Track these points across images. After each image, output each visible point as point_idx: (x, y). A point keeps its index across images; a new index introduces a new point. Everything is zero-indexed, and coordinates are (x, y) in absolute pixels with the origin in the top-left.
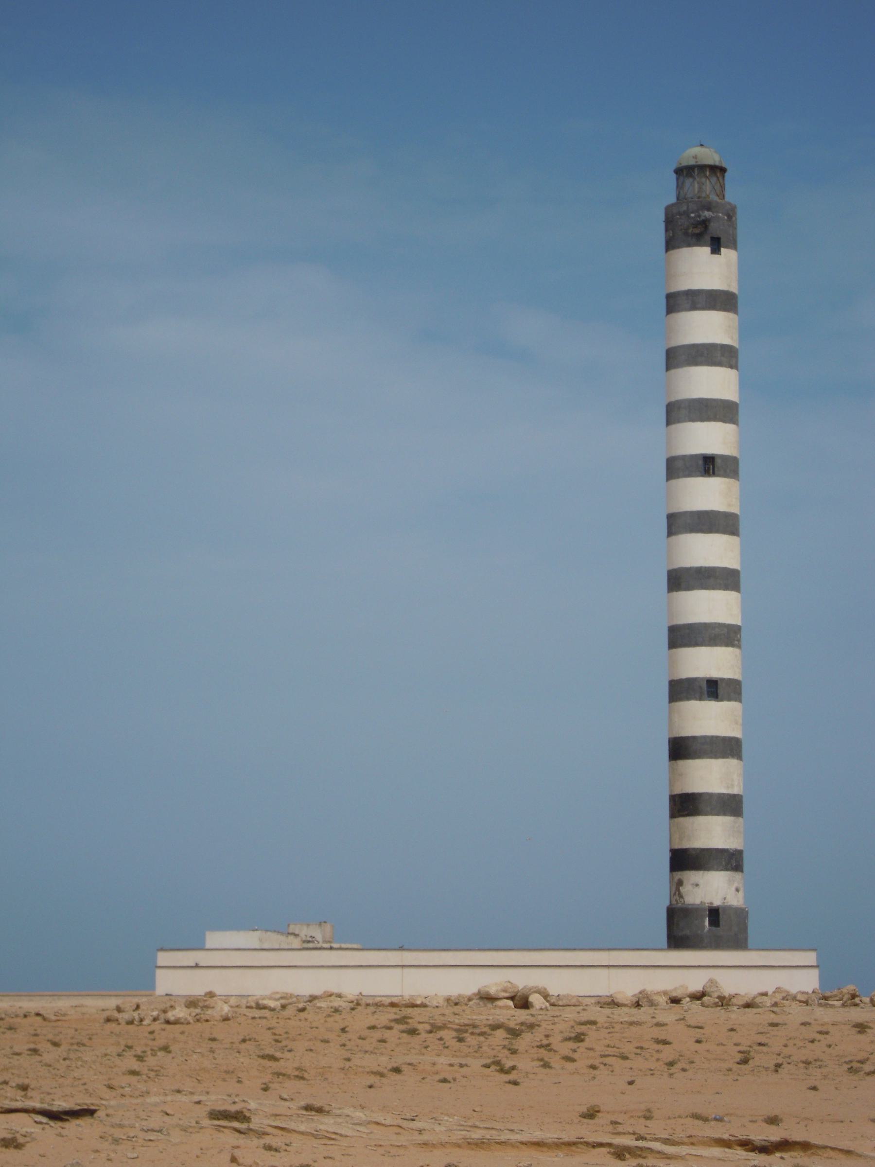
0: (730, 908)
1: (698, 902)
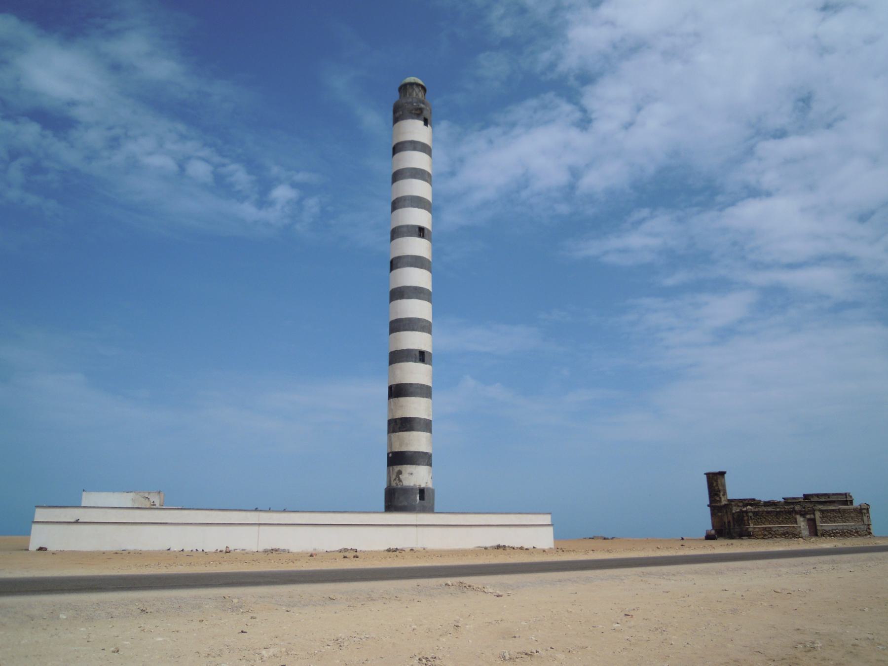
1: (412, 484)
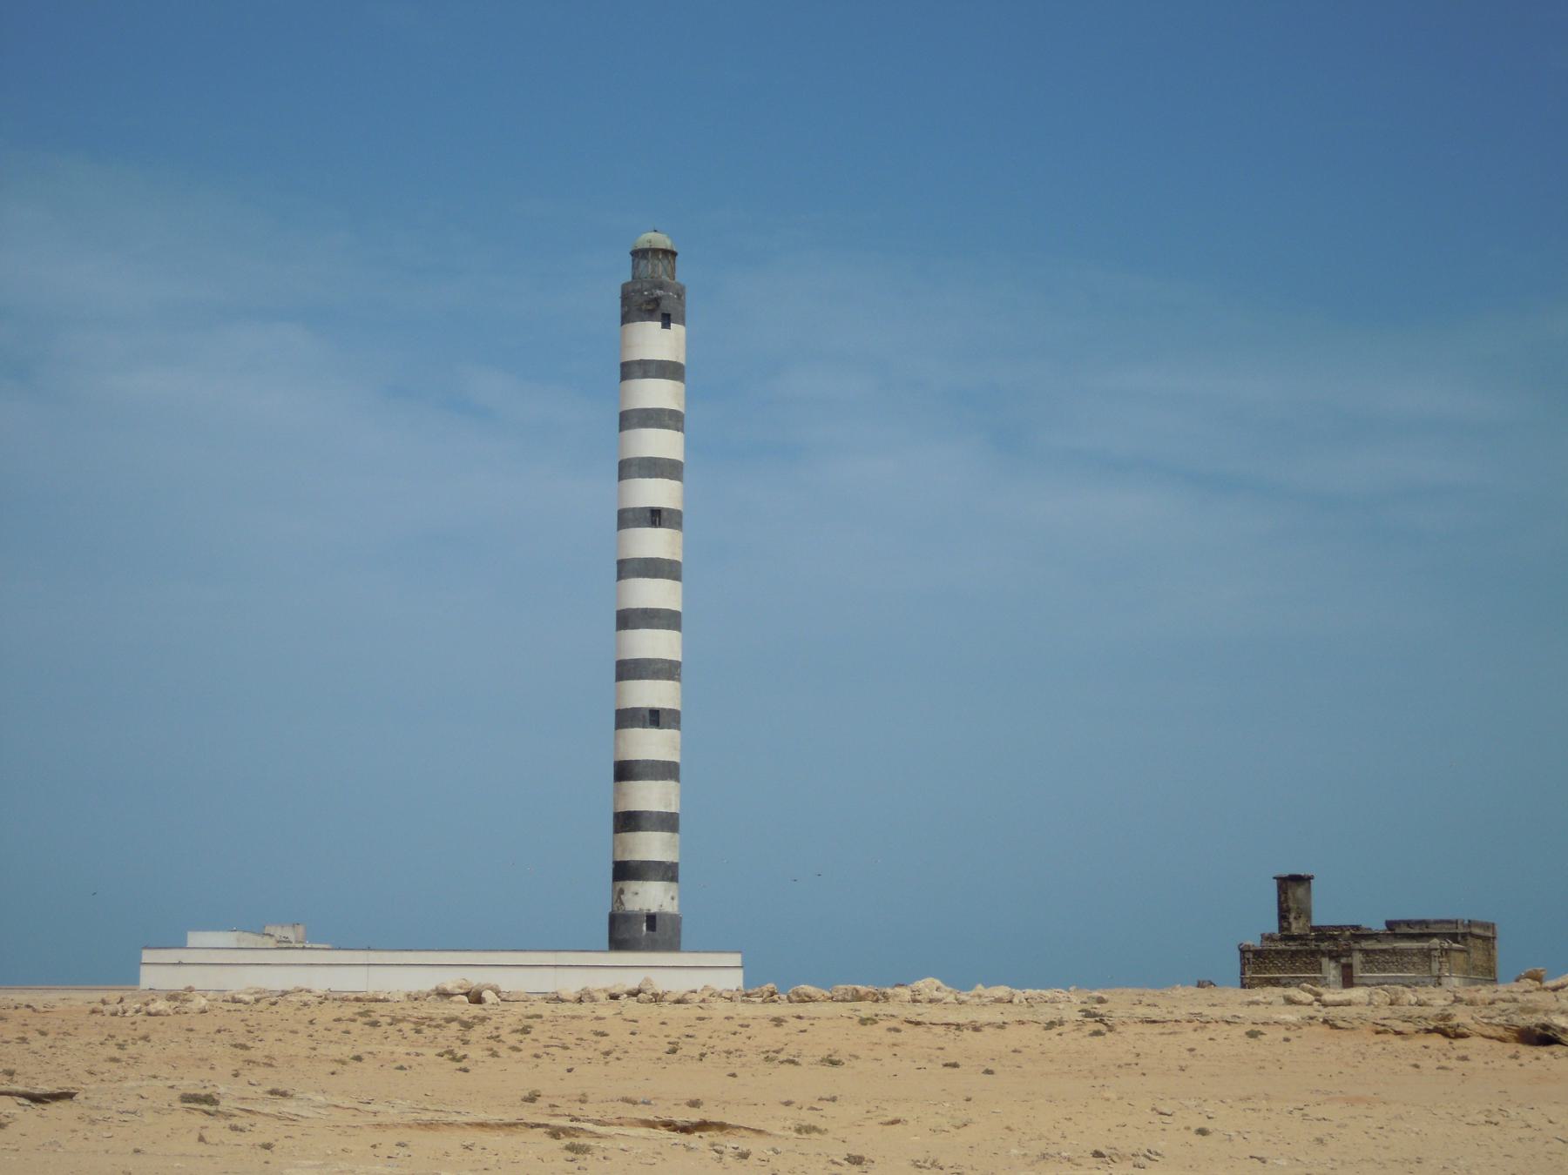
0: (666, 914)
